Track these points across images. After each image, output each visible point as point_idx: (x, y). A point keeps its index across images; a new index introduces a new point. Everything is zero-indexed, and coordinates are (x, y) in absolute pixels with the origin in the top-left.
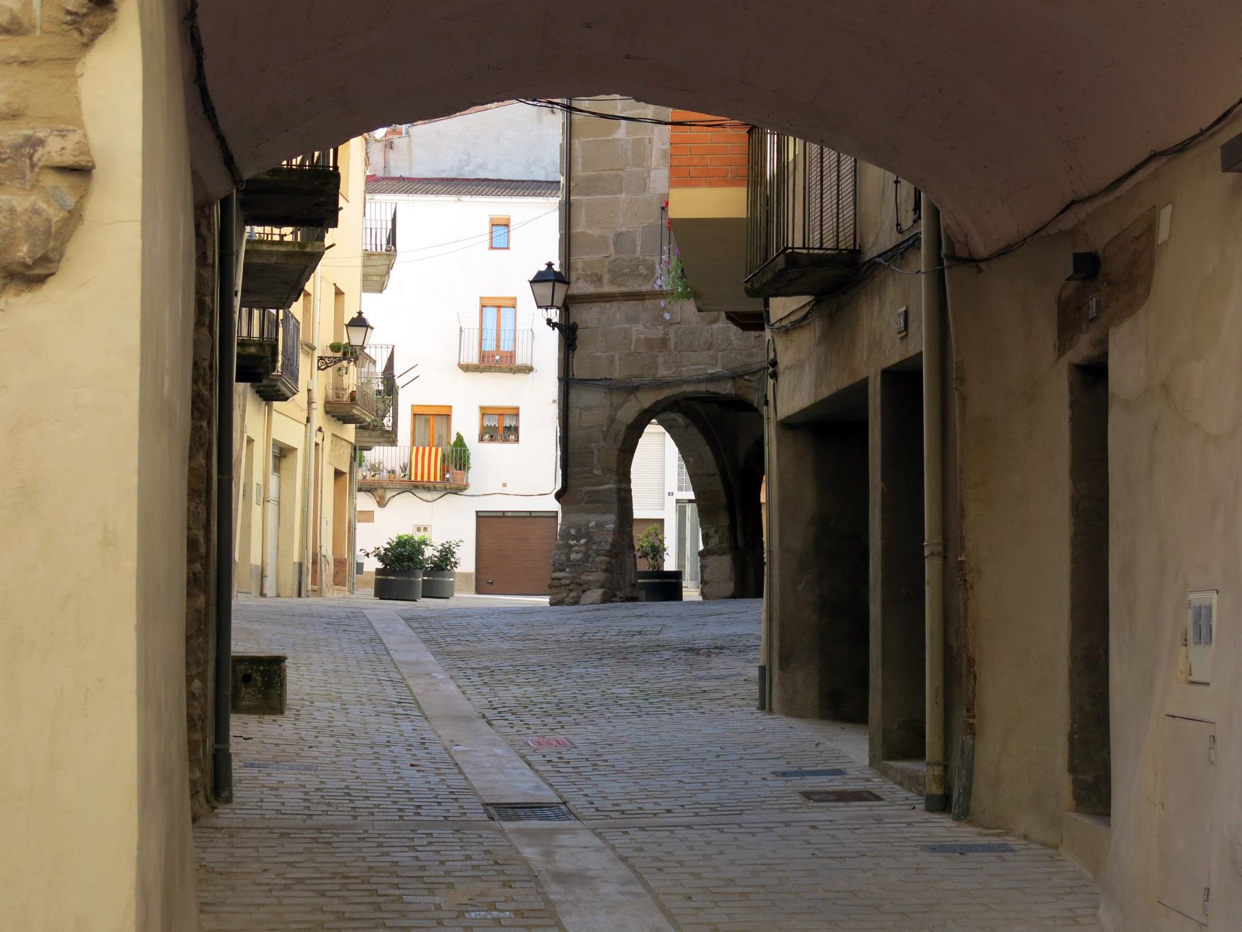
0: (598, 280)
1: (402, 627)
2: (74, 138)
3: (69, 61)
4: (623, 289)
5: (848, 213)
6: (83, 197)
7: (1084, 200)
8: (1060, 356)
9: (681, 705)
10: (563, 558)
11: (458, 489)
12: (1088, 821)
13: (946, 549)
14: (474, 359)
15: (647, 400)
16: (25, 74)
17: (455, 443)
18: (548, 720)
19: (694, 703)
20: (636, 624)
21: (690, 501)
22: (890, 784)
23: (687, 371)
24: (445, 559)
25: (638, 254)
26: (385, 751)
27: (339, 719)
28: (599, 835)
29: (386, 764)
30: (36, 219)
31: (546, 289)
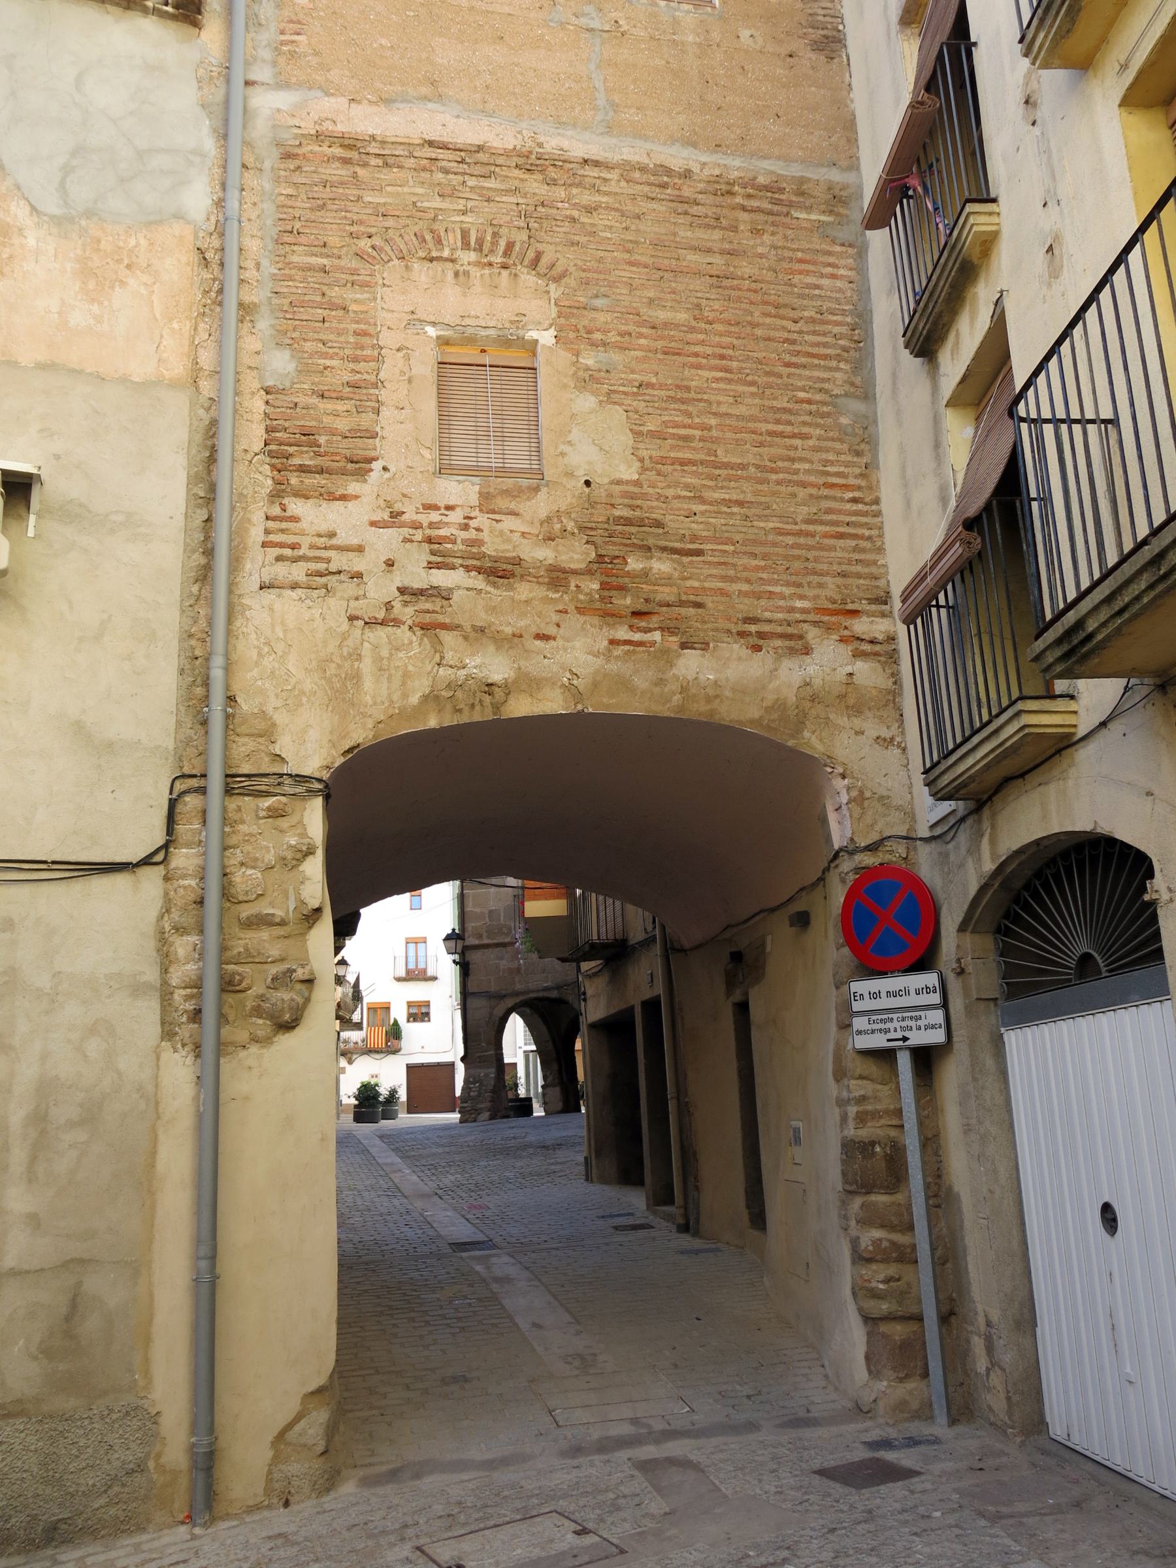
0: (480, 936)
1: (378, 1142)
2: (308, 967)
3: (303, 934)
4: (495, 941)
5: (619, 920)
6: (310, 992)
7: (733, 926)
8: (728, 998)
9: (542, 1181)
10: (467, 1095)
11: (396, 1051)
12: (756, 1233)
13: (678, 1095)
14: (403, 974)
15: (510, 1002)
16: (287, 942)
17: (393, 1025)
18: (472, 1194)
19: (550, 1179)
20: (510, 1133)
21: (532, 1051)
22: (658, 1219)
23: (532, 986)
24: (393, 1093)
25: (502, 922)
26: (388, 1218)
27: (359, 1202)
28: (512, 1256)
29: (391, 1225)
30: (293, 1003)
31: (452, 943)
